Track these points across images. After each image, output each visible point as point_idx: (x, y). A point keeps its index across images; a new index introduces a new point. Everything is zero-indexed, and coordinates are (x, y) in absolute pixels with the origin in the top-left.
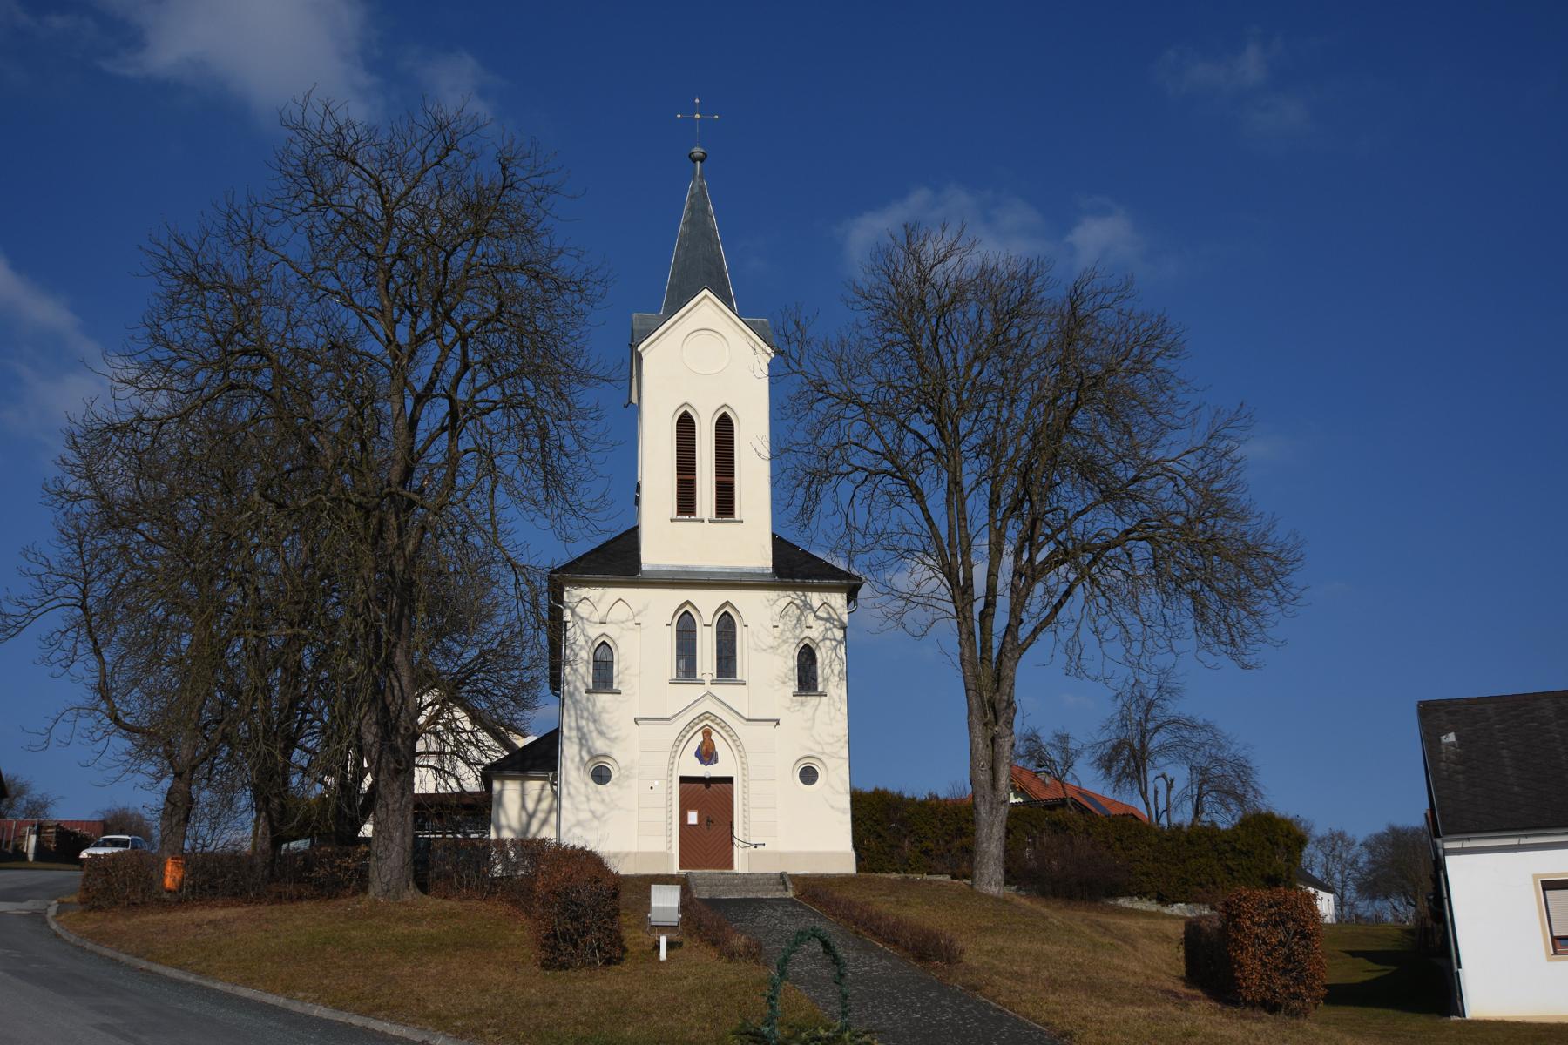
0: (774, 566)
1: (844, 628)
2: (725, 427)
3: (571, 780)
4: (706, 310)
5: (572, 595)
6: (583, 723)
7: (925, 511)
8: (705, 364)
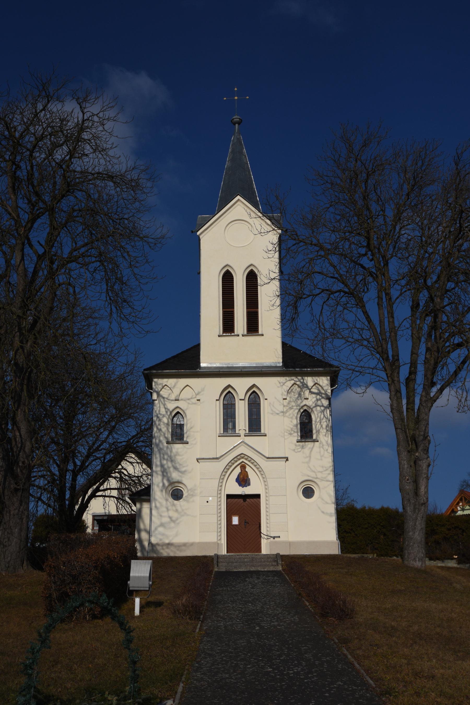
0: (283, 362)
1: (329, 399)
2: (252, 278)
3: (157, 497)
4: (239, 208)
5: (158, 383)
6: (165, 462)
7: (365, 313)
8: (239, 240)
